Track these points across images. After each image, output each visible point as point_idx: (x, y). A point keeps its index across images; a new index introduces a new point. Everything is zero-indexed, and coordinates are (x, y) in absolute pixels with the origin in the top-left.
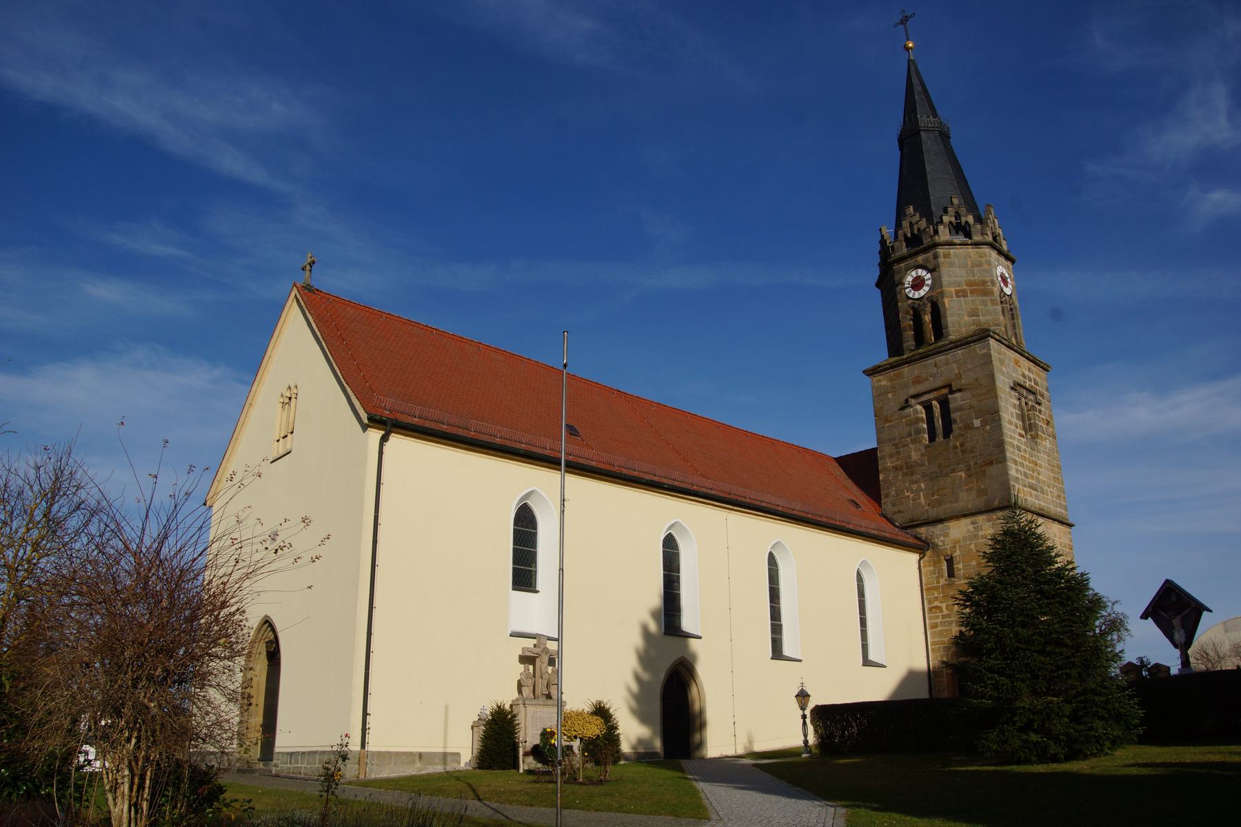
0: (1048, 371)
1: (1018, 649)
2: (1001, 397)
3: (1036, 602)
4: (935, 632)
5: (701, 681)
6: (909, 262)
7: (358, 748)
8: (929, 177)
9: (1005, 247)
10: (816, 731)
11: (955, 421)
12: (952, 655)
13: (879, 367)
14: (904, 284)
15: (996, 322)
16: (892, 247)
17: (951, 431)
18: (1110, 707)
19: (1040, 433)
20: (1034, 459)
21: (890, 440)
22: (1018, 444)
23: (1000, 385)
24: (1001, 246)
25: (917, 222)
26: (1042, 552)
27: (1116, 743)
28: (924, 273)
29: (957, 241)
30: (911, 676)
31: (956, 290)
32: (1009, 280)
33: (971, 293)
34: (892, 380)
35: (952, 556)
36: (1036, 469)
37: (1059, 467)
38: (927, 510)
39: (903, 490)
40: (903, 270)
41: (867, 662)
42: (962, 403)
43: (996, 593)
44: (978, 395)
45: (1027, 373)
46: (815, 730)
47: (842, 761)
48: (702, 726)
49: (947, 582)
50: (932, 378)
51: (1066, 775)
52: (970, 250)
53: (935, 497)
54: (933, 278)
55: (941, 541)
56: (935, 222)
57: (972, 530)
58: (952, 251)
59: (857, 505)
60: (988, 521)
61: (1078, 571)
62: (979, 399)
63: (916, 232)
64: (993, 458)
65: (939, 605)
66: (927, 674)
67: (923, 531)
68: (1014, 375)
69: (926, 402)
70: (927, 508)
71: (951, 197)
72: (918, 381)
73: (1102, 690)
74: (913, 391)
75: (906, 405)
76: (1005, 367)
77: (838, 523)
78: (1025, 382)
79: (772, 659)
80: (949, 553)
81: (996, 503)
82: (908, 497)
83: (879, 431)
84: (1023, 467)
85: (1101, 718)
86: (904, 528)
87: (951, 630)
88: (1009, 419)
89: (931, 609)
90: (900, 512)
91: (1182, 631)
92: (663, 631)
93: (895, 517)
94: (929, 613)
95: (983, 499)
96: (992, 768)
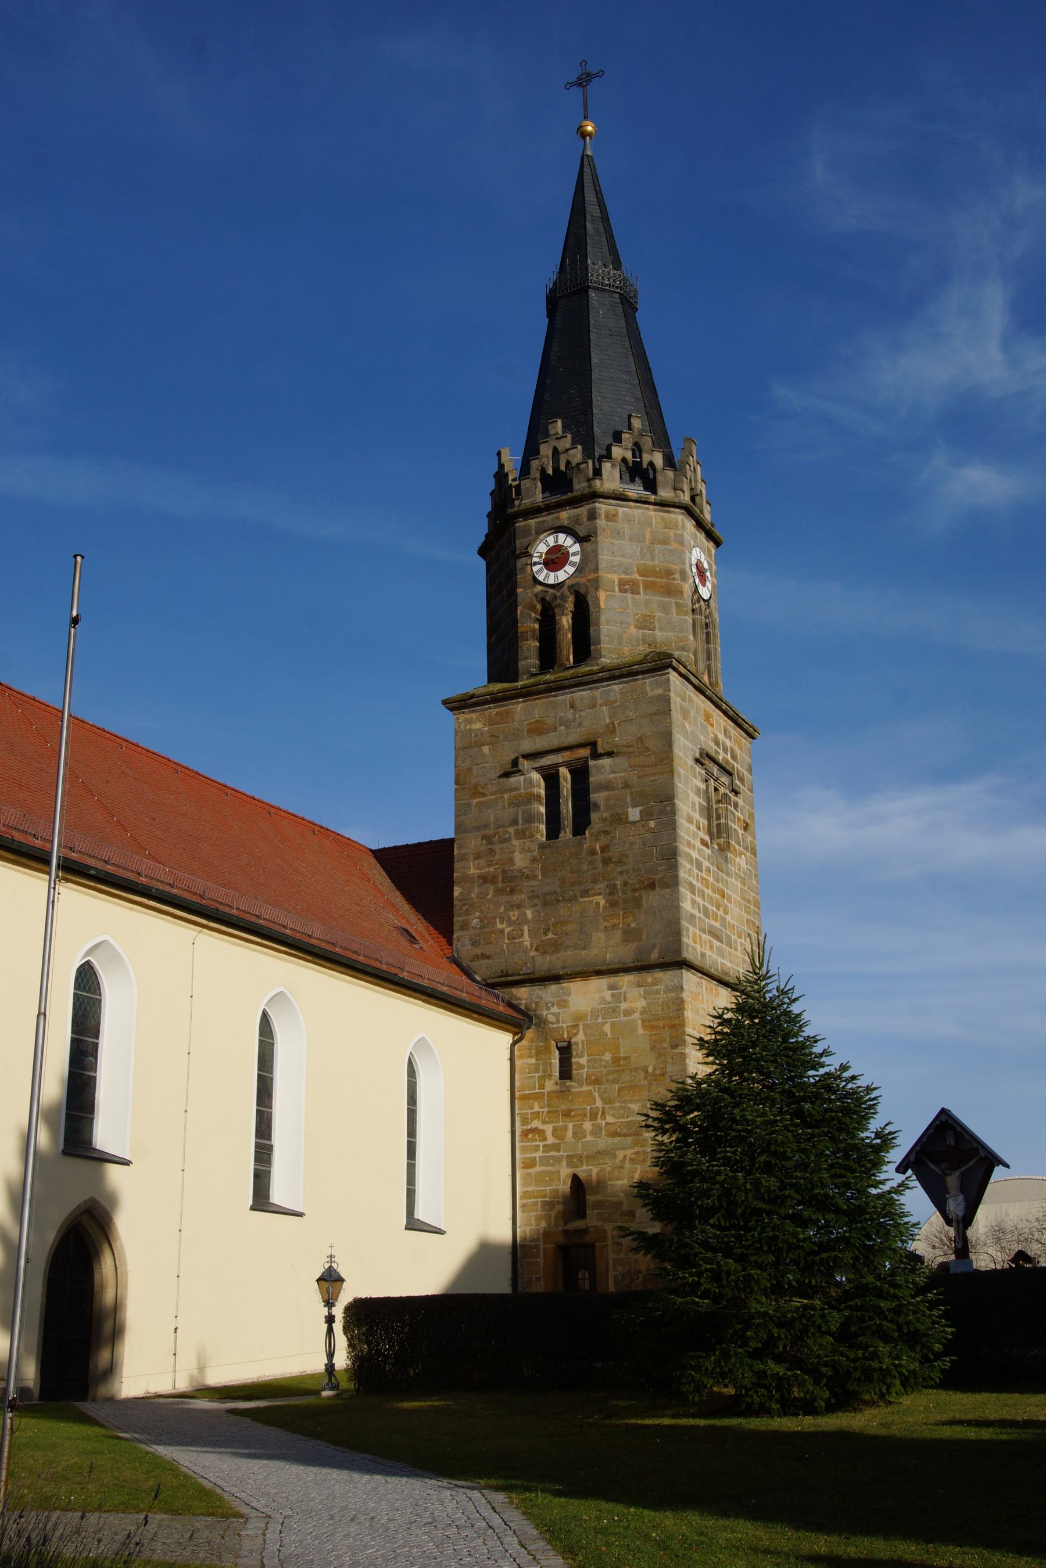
0: (754, 738)
1: (758, 1212)
2: (679, 774)
3: (793, 1132)
4: (529, 1174)
5: (122, 1247)
6: (545, 518)
8: (595, 375)
9: (708, 516)
10: (351, 1345)
11: (597, 806)
12: (556, 1217)
13: (473, 696)
14: (531, 556)
15: (681, 644)
16: (518, 487)
17: (588, 823)
18: (901, 1320)
19: (732, 842)
20: (720, 885)
21: (478, 828)
22: (699, 858)
23: (680, 754)
24: (702, 513)
25: (567, 450)
26: (802, 1046)
27: (910, 1383)
29: (632, 494)
30: (485, 1251)
31: (620, 580)
32: (708, 574)
34: (491, 722)
35: (569, 1042)
36: (721, 903)
37: (757, 904)
38: (533, 958)
39: (494, 918)
40: (533, 532)
41: (413, 1224)
42: (612, 776)
43: (723, 1110)
45: (721, 737)
46: (350, 1345)
47: (407, 1405)
48: (117, 1333)
50: (563, 728)
51: (843, 1436)
52: (652, 513)
54: (583, 552)
55: (553, 1014)
56: (597, 456)
57: (609, 999)
58: (621, 510)
59: (413, 939)
60: (639, 986)
61: (862, 1082)
63: (563, 468)
64: (657, 877)
65: (540, 1126)
67: (523, 994)
68: (702, 738)
70: (533, 953)
71: (630, 416)
72: (537, 729)
73: (892, 1291)
75: (513, 769)
76: (690, 723)
77: (384, 967)
78: (717, 752)
79: (252, 1208)
80: (566, 1036)
81: (654, 956)
82: (502, 931)
83: (461, 810)
84: (703, 898)
85: (886, 1338)
86: (491, 986)
87: (559, 1172)
88: (688, 814)
89: (525, 1134)
90: (484, 956)
91: (961, 1198)
92: (61, 1147)
93: (475, 965)
94: (522, 1141)
95: (633, 946)
96: (702, 1422)
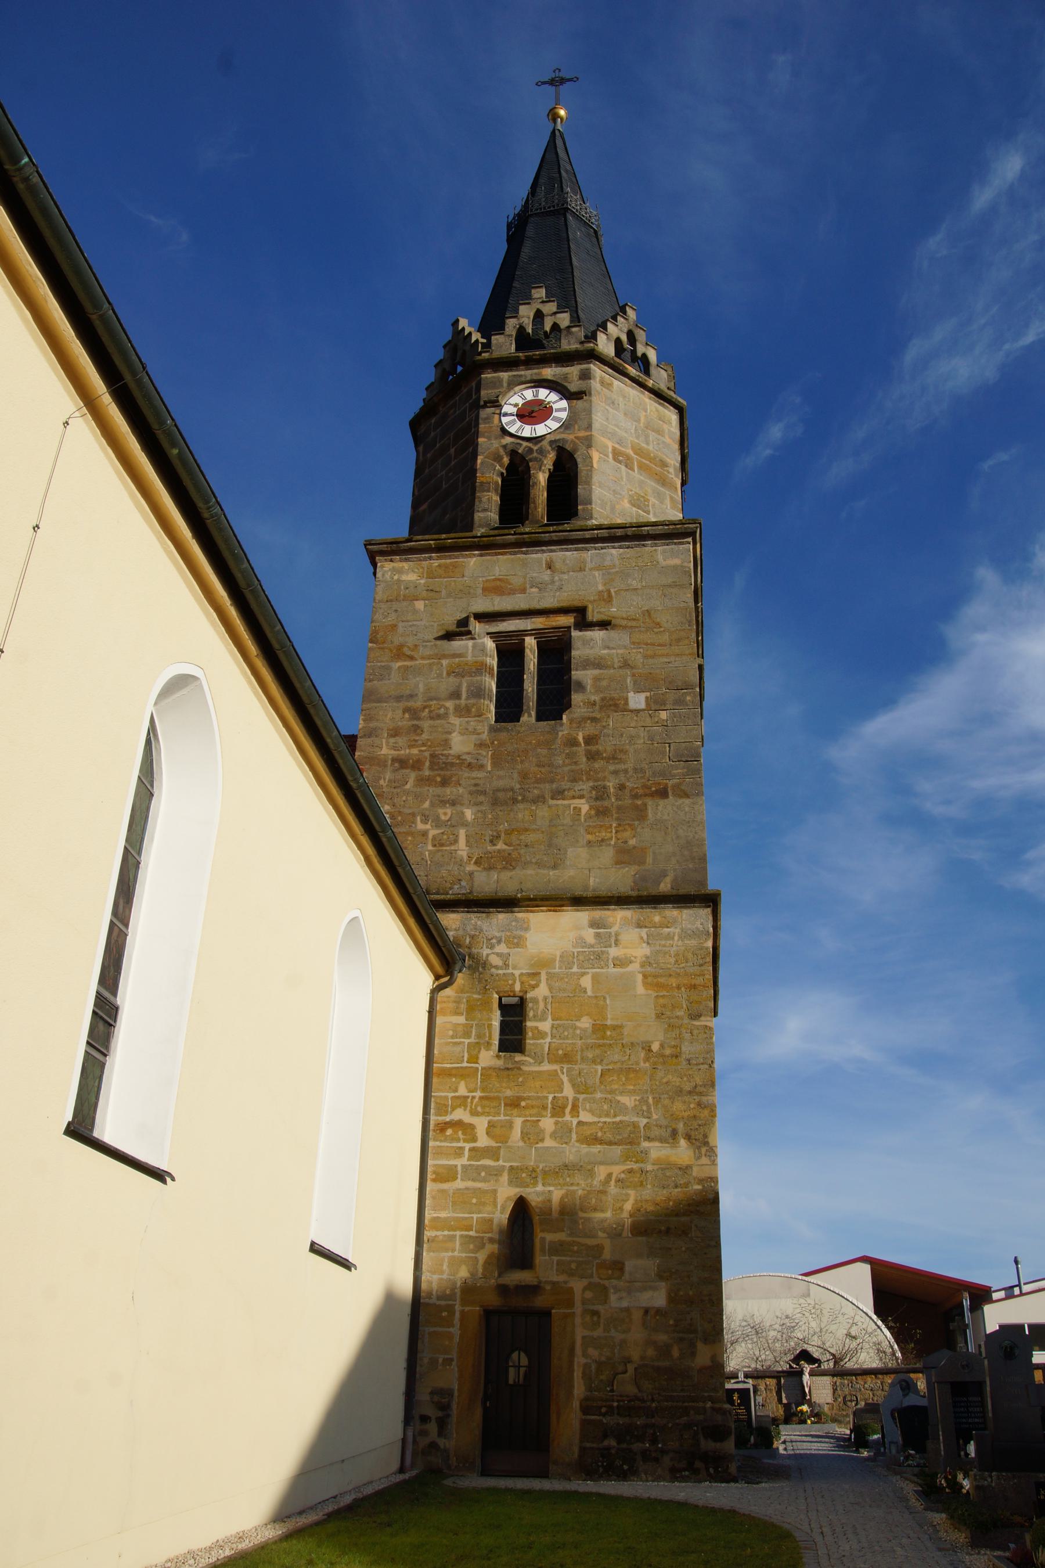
6: (523, 373)
11: (581, 687)
12: (487, 1263)
21: (399, 698)
28: (553, 397)
34: (431, 575)
38: (471, 874)
39: (414, 815)
40: (505, 385)
42: (606, 651)
44: (647, 644)
49: (500, 1063)
50: (534, 590)
52: (647, 400)
53: (498, 847)
55: (498, 954)
58: (616, 383)
62: (650, 653)
64: (670, 783)
65: (467, 1118)
66: (408, 1310)
70: (471, 867)
72: (497, 588)
74: (482, 605)
75: (461, 630)
81: (665, 887)
82: (425, 834)
87: (495, 1192)
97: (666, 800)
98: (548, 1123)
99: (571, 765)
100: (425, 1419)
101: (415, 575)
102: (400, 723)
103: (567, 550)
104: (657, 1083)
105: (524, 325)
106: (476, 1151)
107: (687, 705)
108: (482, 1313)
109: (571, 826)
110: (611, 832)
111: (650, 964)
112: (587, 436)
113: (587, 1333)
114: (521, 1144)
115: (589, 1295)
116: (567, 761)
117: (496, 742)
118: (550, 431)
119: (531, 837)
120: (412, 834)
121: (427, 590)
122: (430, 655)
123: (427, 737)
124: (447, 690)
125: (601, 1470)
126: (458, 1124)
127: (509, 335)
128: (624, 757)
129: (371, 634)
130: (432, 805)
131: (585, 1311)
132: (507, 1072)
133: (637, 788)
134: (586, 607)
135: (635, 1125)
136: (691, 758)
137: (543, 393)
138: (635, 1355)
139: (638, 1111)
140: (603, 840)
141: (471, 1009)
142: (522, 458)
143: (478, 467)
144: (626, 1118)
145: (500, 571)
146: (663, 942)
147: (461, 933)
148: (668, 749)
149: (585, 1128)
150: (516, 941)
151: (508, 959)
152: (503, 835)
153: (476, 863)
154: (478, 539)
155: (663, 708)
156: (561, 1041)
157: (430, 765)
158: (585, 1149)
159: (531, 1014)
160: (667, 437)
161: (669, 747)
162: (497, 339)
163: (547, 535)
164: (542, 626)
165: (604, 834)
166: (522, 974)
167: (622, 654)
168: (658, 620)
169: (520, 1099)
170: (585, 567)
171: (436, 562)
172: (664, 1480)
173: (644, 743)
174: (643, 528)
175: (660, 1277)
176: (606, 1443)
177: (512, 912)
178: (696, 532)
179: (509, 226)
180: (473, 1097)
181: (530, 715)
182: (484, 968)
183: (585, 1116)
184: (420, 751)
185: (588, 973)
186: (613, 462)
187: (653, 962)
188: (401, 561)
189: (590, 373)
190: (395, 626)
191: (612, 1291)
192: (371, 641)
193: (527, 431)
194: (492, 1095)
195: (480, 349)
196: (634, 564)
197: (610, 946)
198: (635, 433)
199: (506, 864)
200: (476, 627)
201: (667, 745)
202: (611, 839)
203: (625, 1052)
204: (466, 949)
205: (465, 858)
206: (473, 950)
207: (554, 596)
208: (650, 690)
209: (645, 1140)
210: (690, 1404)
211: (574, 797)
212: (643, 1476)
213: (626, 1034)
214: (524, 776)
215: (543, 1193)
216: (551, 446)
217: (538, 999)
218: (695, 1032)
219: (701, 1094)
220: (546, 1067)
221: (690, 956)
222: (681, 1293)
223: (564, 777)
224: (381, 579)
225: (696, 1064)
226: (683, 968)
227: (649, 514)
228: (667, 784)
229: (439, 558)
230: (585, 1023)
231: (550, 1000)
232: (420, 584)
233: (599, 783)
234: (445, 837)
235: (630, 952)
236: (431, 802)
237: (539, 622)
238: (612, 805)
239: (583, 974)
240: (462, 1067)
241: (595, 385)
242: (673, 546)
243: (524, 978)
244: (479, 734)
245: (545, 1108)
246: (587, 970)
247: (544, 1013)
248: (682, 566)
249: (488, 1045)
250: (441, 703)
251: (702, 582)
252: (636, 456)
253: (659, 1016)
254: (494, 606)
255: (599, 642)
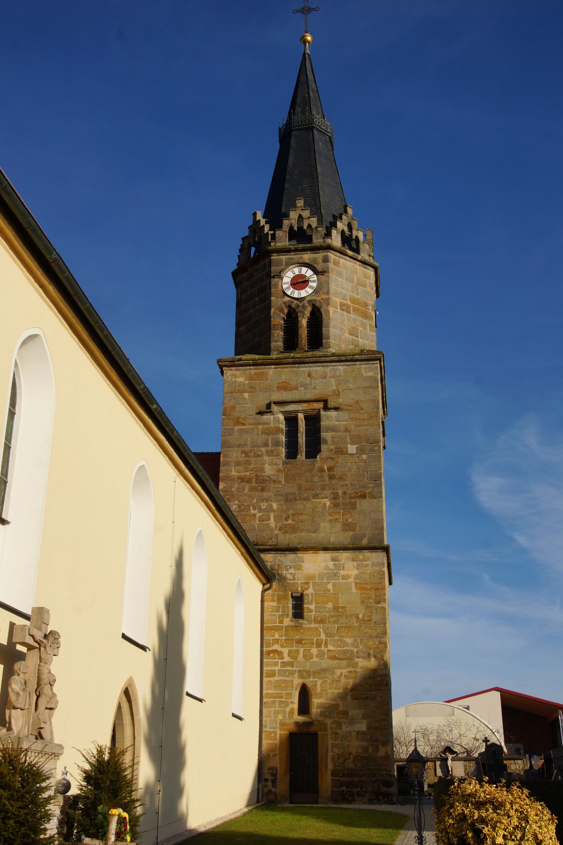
6: (293, 257)
7: (425, 834)
11: (326, 442)
21: (239, 446)
33: (354, 311)
34: (251, 378)
38: (277, 535)
39: (249, 506)
40: (284, 264)
42: (337, 423)
49: (293, 624)
50: (302, 388)
52: (358, 267)
55: (290, 574)
58: (342, 260)
64: (367, 491)
69: (291, 412)
72: (284, 387)
74: (277, 396)
80: (300, 589)
81: (365, 542)
82: (254, 515)
87: (292, 681)
97: (365, 500)
98: (314, 651)
99: (321, 481)
100: (266, 780)
101: (243, 378)
102: (240, 459)
103: (318, 366)
104: (362, 633)
105: (293, 225)
106: (284, 663)
107: (375, 452)
108: (288, 734)
109: (322, 512)
110: (340, 515)
111: (358, 578)
112: (327, 298)
113: (333, 742)
114: (303, 660)
115: (333, 726)
116: (320, 480)
117: (286, 470)
118: (308, 294)
119: (305, 517)
120: (248, 515)
121: (250, 387)
122: (253, 423)
123: (253, 467)
124: (262, 442)
125: (340, 800)
126: (275, 651)
127: (285, 231)
128: (346, 478)
129: (223, 411)
130: (257, 501)
131: (332, 733)
132: (297, 627)
133: (352, 493)
134: (327, 400)
135: (352, 651)
136: (377, 479)
137: (304, 270)
138: (354, 752)
139: (353, 645)
140: (336, 519)
141: (279, 599)
142: (294, 310)
143: (272, 315)
144: (348, 648)
145: (285, 377)
146: (364, 568)
147: (273, 563)
148: (366, 474)
149: (330, 652)
150: (298, 567)
151: (295, 576)
152: (291, 516)
153: (279, 530)
154: (274, 360)
155: (364, 453)
156: (319, 614)
157: (255, 481)
158: (330, 662)
159: (306, 601)
160: (368, 287)
161: (367, 473)
162: (278, 234)
163: (308, 359)
164: (306, 409)
165: (337, 516)
166: (301, 583)
167: (345, 424)
168: (362, 406)
169: (302, 640)
170: (327, 376)
171: (253, 371)
172: (366, 804)
173: (355, 471)
174: (355, 356)
175: (364, 717)
176: (342, 788)
177: (296, 554)
178: (381, 359)
179: (280, 130)
180: (282, 639)
181: (302, 455)
182: (284, 580)
183: (330, 647)
184: (250, 473)
185: (331, 582)
186: (340, 311)
187: (359, 577)
188: (236, 370)
189: (328, 258)
190: (235, 407)
191: (343, 724)
192: (223, 415)
193: (296, 294)
194: (289, 638)
195: (270, 240)
196: (351, 375)
197: (340, 570)
198: (352, 289)
199: (293, 530)
200: (275, 408)
201: (366, 472)
202: (340, 518)
203: (347, 618)
204: (276, 571)
205: (274, 527)
206: (279, 571)
207: (312, 392)
208: (358, 444)
209: (356, 658)
210: (377, 772)
211: (323, 498)
212: (358, 802)
213: (347, 610)
214: (300, 487)
215: (313, 681)
216: (308, 303)
217: (309, 595)
218: (378, 610)
219: (380, 637)
220: (313, 625)
221: (376, 575)
222: (373, 725)
223: (318, 488)
224: (226, 380)
225: (379, 624)
226: (373, 580)
227: (358, 338)
228: (366, 492)
229: (254, 369)
230: (330, 605)
231: (314, 595)
232: (246, 383)
233: (335, 491)
234: (264, 517)
235: (350, 573)
236: (257, 499)
237: (304, 406)
238: (341, 502)
239: (329, 583)
240: (276, 626)
241: (331, 265)
242: (370, 365)
243: (303, 585)
244: (278, 465)
245: (313, 644)
246: (330, 581)
247: (311, 601)
248: (374, 377)
249: (287, 615)
250: (259, 449)
251: (384, 374)
252: (352, 304)
253: (362, 602)
254: (283, 397)
255: (334, 418)
